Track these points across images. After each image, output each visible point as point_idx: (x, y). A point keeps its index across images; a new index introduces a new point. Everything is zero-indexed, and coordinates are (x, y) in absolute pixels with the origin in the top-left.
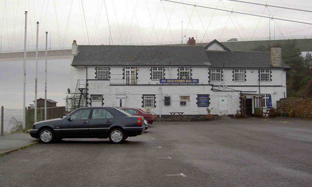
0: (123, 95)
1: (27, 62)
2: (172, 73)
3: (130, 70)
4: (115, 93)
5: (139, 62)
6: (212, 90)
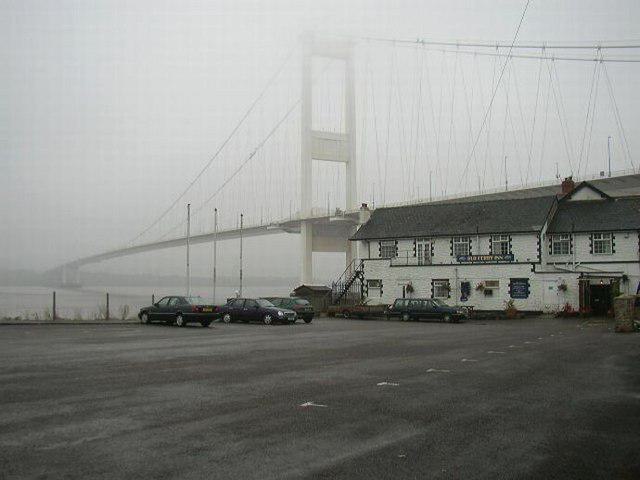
0: (397, 277)
1: (218, 242)
2: (482, 246)
3: (423, 243)
4: (396, 277)
5: (438, 230)
6: (533, 270)
